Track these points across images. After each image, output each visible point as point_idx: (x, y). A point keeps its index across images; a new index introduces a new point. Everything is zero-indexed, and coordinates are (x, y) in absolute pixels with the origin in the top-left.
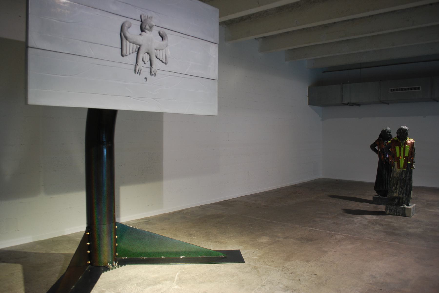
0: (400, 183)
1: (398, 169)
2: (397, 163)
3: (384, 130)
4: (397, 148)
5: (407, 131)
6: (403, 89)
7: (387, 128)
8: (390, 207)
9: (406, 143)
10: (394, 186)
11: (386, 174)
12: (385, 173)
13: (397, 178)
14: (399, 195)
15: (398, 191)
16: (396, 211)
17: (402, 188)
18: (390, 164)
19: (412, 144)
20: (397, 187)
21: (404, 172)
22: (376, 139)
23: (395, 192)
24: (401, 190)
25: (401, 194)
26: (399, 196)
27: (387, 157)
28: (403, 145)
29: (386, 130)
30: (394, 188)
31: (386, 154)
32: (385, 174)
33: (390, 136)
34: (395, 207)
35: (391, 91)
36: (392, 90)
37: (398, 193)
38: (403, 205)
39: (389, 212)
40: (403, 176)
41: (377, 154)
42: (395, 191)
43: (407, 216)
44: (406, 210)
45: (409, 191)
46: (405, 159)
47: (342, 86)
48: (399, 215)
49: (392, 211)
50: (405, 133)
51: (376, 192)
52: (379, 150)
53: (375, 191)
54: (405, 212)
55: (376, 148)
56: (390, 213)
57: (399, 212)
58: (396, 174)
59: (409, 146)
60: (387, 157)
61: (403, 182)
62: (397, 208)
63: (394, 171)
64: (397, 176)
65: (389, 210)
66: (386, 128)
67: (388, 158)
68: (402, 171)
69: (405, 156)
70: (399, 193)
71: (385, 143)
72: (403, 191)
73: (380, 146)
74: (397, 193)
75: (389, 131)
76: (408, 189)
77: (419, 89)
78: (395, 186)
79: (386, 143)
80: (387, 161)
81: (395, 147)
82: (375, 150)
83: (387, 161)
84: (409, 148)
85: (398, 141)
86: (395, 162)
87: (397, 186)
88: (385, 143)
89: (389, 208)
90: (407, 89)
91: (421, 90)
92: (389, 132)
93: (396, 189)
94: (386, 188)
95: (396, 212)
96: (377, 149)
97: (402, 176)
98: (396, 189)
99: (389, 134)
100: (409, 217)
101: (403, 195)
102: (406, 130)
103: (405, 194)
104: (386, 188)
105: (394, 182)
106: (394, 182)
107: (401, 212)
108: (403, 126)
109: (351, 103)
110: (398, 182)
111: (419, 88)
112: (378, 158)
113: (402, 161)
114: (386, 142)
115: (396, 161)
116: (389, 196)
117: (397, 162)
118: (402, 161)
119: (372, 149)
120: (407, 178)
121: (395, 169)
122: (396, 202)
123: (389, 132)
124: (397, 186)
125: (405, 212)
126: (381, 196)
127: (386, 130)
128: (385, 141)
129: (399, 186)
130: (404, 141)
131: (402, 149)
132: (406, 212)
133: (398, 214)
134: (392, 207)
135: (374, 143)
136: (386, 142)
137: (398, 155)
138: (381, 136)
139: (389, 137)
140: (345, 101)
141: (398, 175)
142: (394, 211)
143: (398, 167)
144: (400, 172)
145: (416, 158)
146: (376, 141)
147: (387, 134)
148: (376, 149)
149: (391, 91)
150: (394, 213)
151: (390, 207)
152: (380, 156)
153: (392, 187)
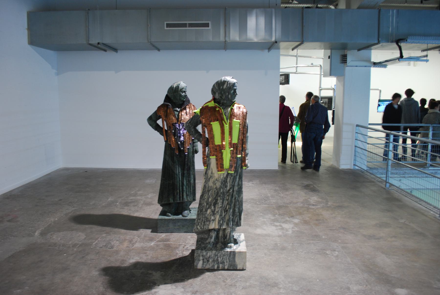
0: (221, 201)
1: (218, 171)
2: (217, 160)
3: (175, 86)
4: (216, 126)
5: (235, 88)
6: (184, 25)
7: (179, 83)
8: (205, 254)
9: (232, 115)
10: (210, 207)
11: (180, 174)
12: (178, 172)
13: (216, 191)
14: (221, 225)
15: (218, 217)
16: (218, 260)
17: (226, 211)
18: (187, 153)
19: (244, 116)
20: (216, 210)
21: (230, 178)
22: (159, 105)
23: (213, 220)
24: (225, 216)
25: (225, 224)
26: (221, 227)
27: (181, 142)
28: (227, 120)
29: (178, 87)
30: (209, 211)
31: (179, 135)
32: (179, 173)
33: (185, 100)
34: (214, 252)
35: (167, 27)
36: (168, 25)
37: (219, 221)
38: (229, 245)
39: (203, 264)
40: (228, 185)
41: (162, 134)
42: (212, 218)
43: (238, 268)
44: (237, 255)
45: (238, 214)
46: (232, 149)
47: (88, 13)
48: (224, 269)
49: (208, 261)
50: (232, 92)
51: (161, 206)
52: (166, 128)
53: (160, 205)
54: (234, 261)
55: (160, 122)
56: (204, 266)
57: (223, 263)
58: (214, 183)
59: (239, 121)
60: (182, 141)
61: (227, 198)
62: (219, 254)
63: (209, 177)
64: (215, 187)
65: (203, 260)
66: (177, 83)
67: (184, 141)
68: (225, 175)
69: (233, 142)
70: (221, 222)
71: (177, 113)
72: (227, 218)
73: (166, 118)
74: (217, 223)
75: (183, 89)
76: (237, 210)
77: (208, 27)
78: (213, 208)
79: (179, 112)
80: (182, 148)
81: (211, 123)
82: (157, 128)
83: (182, 148)
84: (240, 124)
85: (217, 109)
86: (211, 157)
87: (215, 207)
88: (177, 113)
89: (202, 256)
90: (191, 25)
91: (210, 28)
92: (184, 90)
93: (214, 213)
94: (181, 199)
95: (218, 263)
96: (162, 127)
97: (226, 187)
98: (214, 213)
99: (183, 94)
100: (243, 270)
101: (228, 224)
102: (234, 85)
103: (232, 223)
104: (181, 199)
105: (210, 200)
106: (210, 200)
107: (227, 262)
108: (227, 76)
109: (104, 44)
110: (219, 199)
111: (207, 25)
112: (164, 143)
113: (226, 155)
114: (177, 111)
115: (213, 155)
116: (198, 227)
117: (216, 156)
118: (226, 155)
119: (150, 125)
120: (236, 188)
121: (212, 173)
122: (213, 238)
123: (185, 92)
124: (215, 207)
125: (234, 261)
126: (172, 214)
127: (178, 87)
128: (175, 109)
129: (221, 207)
130: (229, 109)
131: (227, 127)
132: (238, 261)
133: (221, 266)
134: (208, 254)
135: (156, 113)
136: (179, 110)
137: (217, 141)
138: (167, 98)
139: (184, 101)
140: (94, 41)
141: (218, 185)
142: (214, 261)
143: (218, 168)
144: (222, 177)
145: (250, 146)
146: (159, 108)
147: (180, 93)
148: (158, 125)
149: (167, 27)
150: (214, 266)
151: (205, 254)
152: (167, 139)
153: (206, 211)
